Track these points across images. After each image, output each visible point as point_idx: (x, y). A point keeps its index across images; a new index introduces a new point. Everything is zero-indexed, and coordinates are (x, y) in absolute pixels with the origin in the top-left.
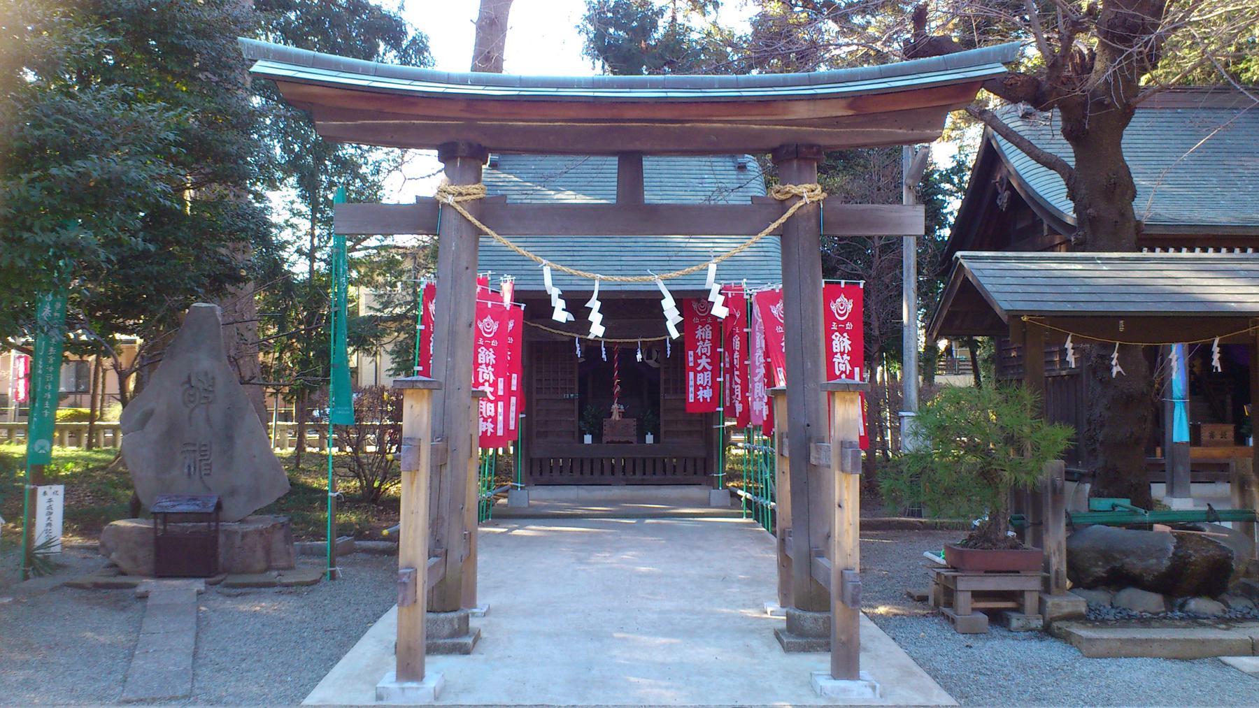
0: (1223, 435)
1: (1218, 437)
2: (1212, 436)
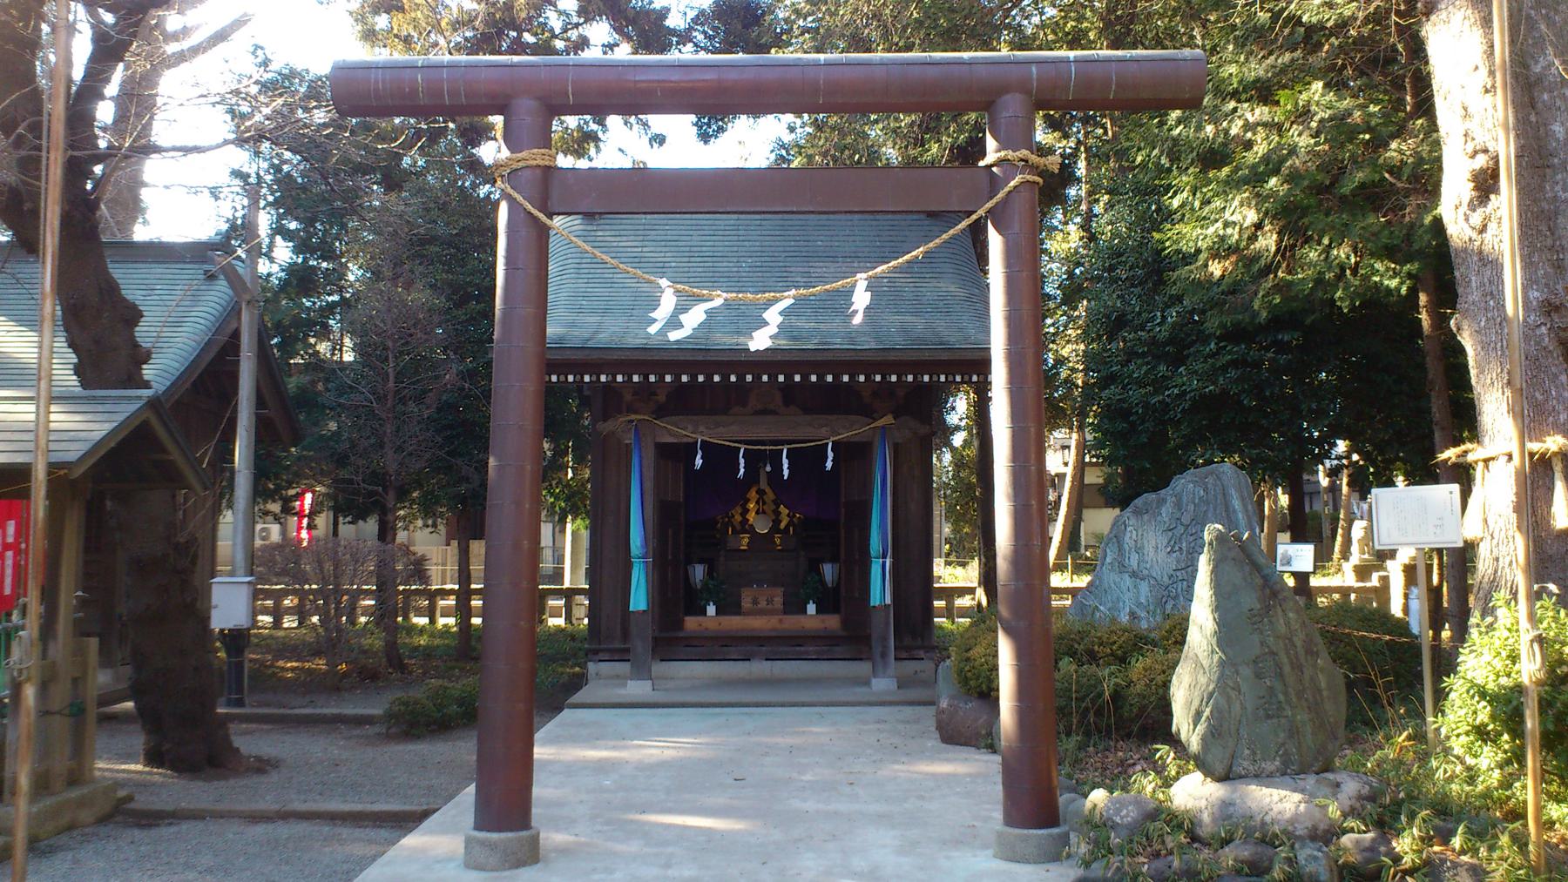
0: (769, 602)
1: (763, 604)
2: (755, 602)
